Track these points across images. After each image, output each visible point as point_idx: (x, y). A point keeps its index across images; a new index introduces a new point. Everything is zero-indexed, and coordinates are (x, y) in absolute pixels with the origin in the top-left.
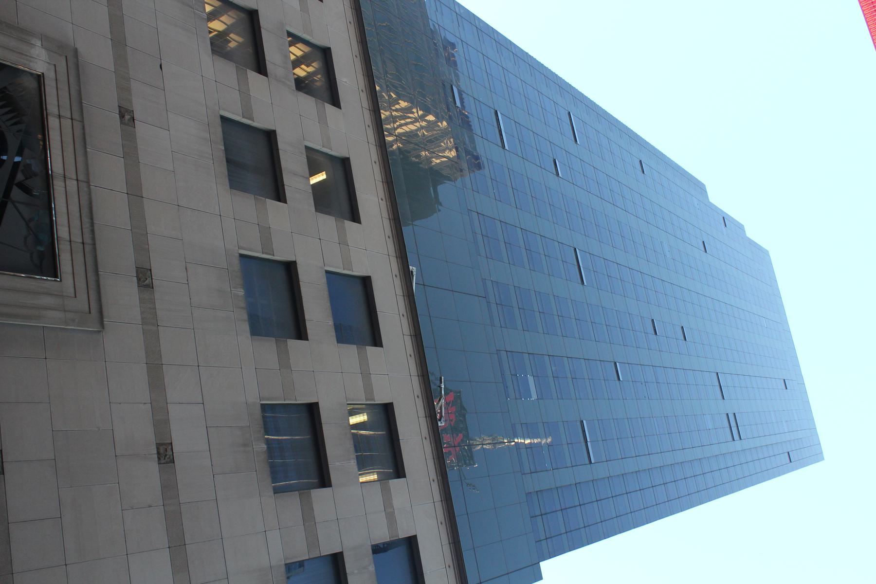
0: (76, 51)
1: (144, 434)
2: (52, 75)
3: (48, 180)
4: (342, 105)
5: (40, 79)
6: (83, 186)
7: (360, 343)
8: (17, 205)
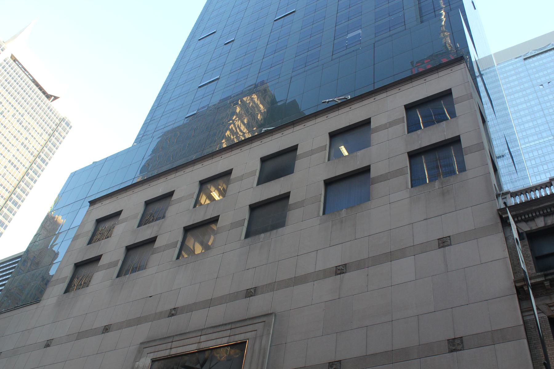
0: (141, 343)
1: (331, 282)
2: (152, 354)
3: (201, 351)
5: (153, 361)
6: (204, 332)
8: (212, 365)
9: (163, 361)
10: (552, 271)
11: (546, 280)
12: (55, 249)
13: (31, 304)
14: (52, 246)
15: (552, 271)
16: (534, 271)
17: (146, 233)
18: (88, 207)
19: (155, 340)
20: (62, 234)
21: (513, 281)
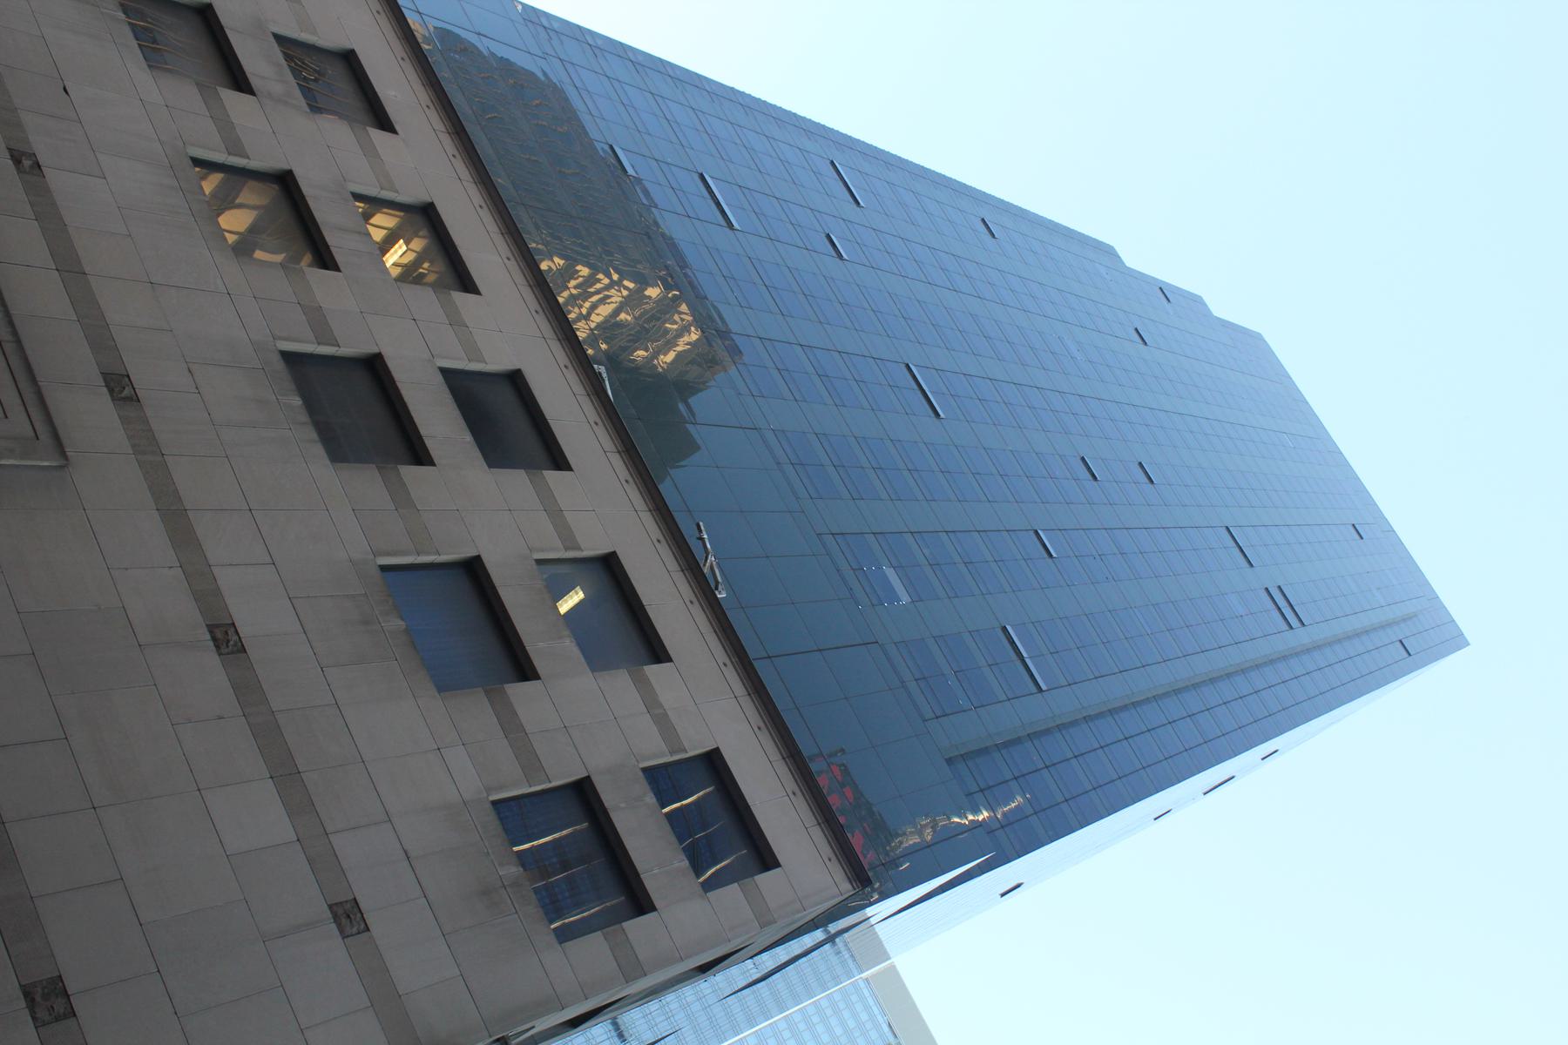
1: (186, 617)
4: (397, 127)
7: (529, 465)
17: (257, 59)
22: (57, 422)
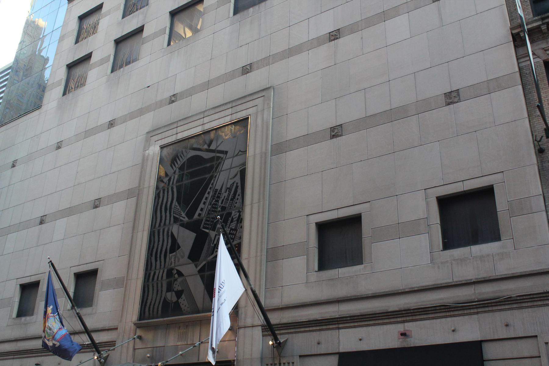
0: (148, 133)
1: (327, 48)
2: (159, 141)
5: (162, 147)
6: (206, 114)
9: (171, 147)
10: (547, 15)
11: (543, 24)
12: (43, 54)
13: (33, 111)
14: (40, 51)
15: (547, 15)
16: (531, 15)
17: (131, 24)
18: (67, 5)
19: (160, 128)
20: (47, 36)
21: (509, 28)
22: (198, 112)
